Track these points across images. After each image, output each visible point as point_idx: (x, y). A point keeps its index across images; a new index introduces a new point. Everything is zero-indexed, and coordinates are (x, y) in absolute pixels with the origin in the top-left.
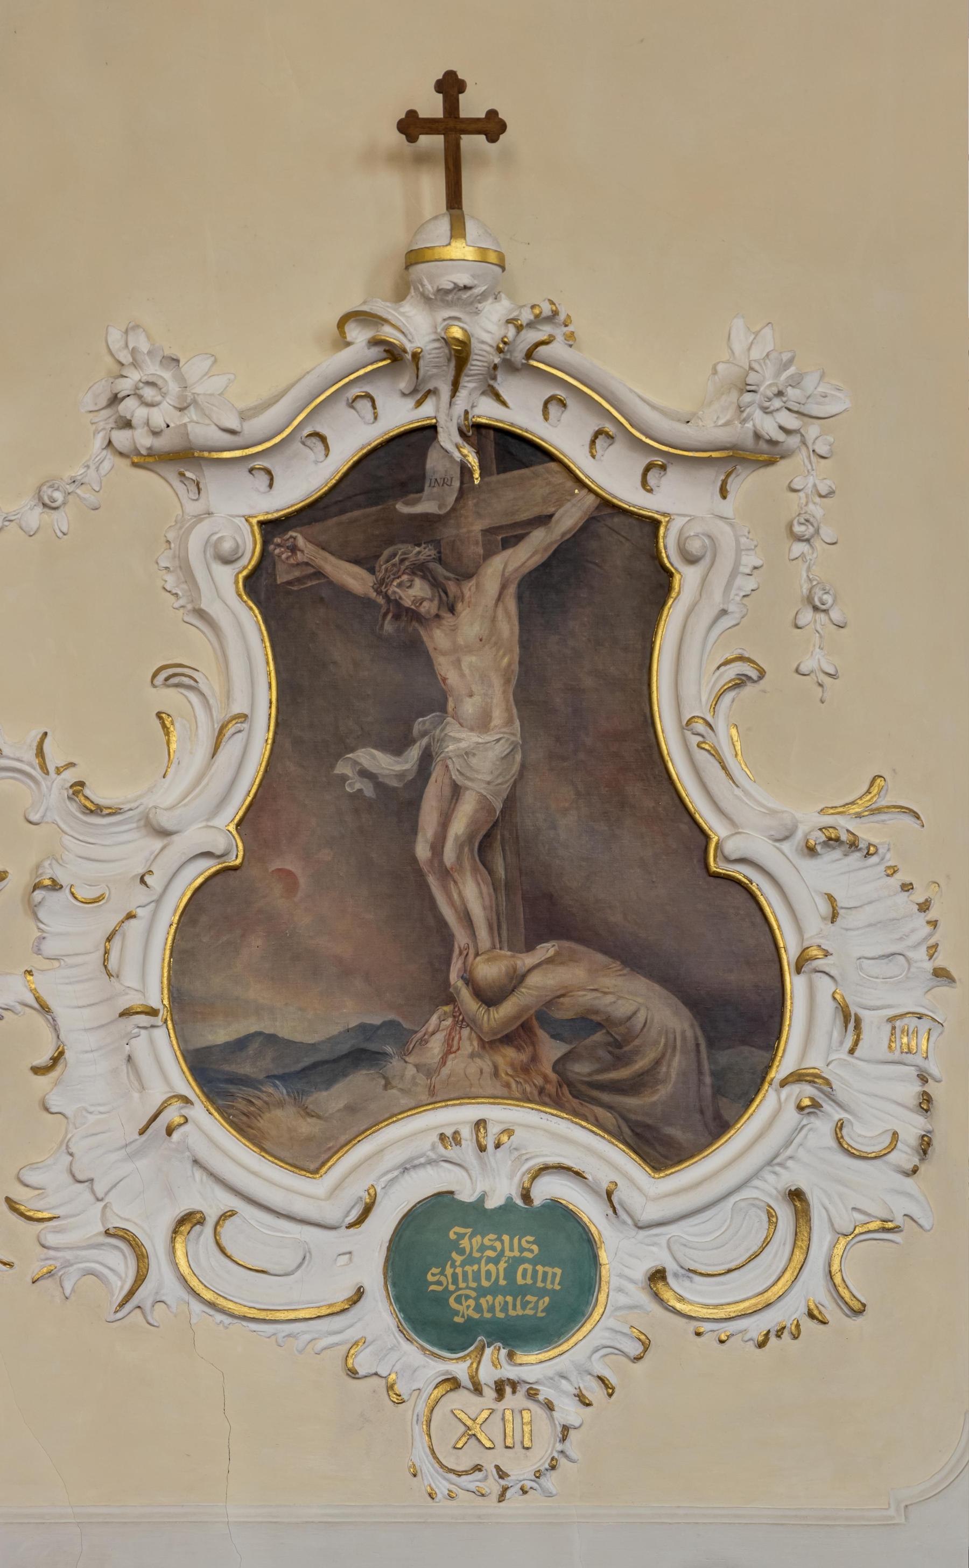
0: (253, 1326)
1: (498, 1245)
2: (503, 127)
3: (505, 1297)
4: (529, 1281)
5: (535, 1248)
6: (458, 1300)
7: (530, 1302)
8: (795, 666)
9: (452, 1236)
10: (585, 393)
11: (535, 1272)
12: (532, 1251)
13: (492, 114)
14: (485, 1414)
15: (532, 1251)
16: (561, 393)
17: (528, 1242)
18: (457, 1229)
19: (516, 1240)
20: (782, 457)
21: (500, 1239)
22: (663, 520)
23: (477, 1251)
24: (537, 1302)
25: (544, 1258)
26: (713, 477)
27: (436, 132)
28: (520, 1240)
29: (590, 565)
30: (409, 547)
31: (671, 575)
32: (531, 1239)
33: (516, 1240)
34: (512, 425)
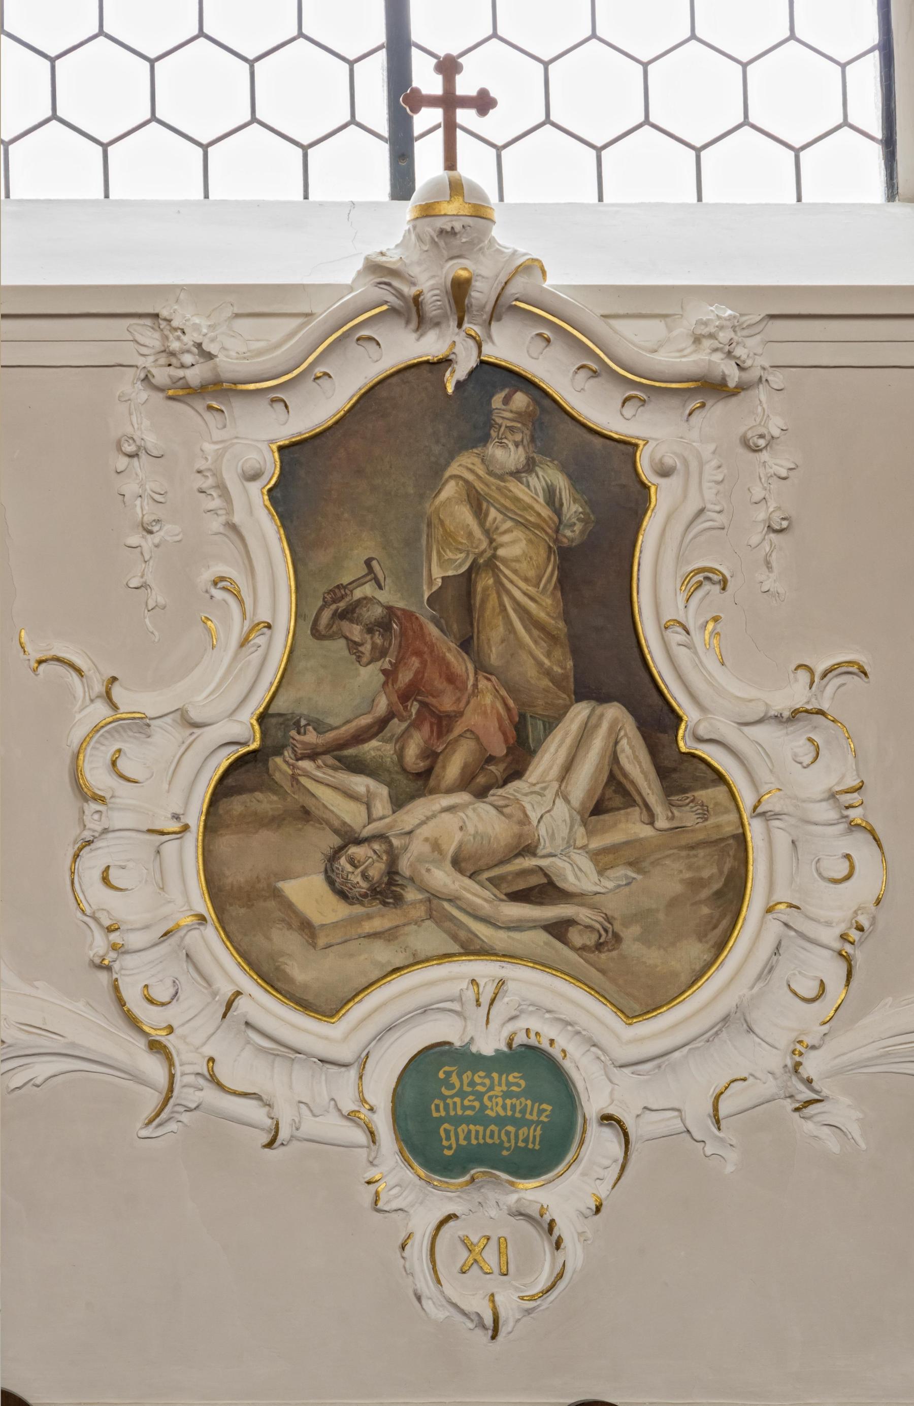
0: (572, 973)
1: (487, 1081)
5: (523, 1083)
7: (546, 1110)
8: (125, 583)
10: (569, 332)
12: (518, 1085)
15: (518, 1085)
16: (547, 333)
19: (504, 1076)
21: (488, 1076)
27: (454, 113)
28: (507, 1076)
31: (648, 488)
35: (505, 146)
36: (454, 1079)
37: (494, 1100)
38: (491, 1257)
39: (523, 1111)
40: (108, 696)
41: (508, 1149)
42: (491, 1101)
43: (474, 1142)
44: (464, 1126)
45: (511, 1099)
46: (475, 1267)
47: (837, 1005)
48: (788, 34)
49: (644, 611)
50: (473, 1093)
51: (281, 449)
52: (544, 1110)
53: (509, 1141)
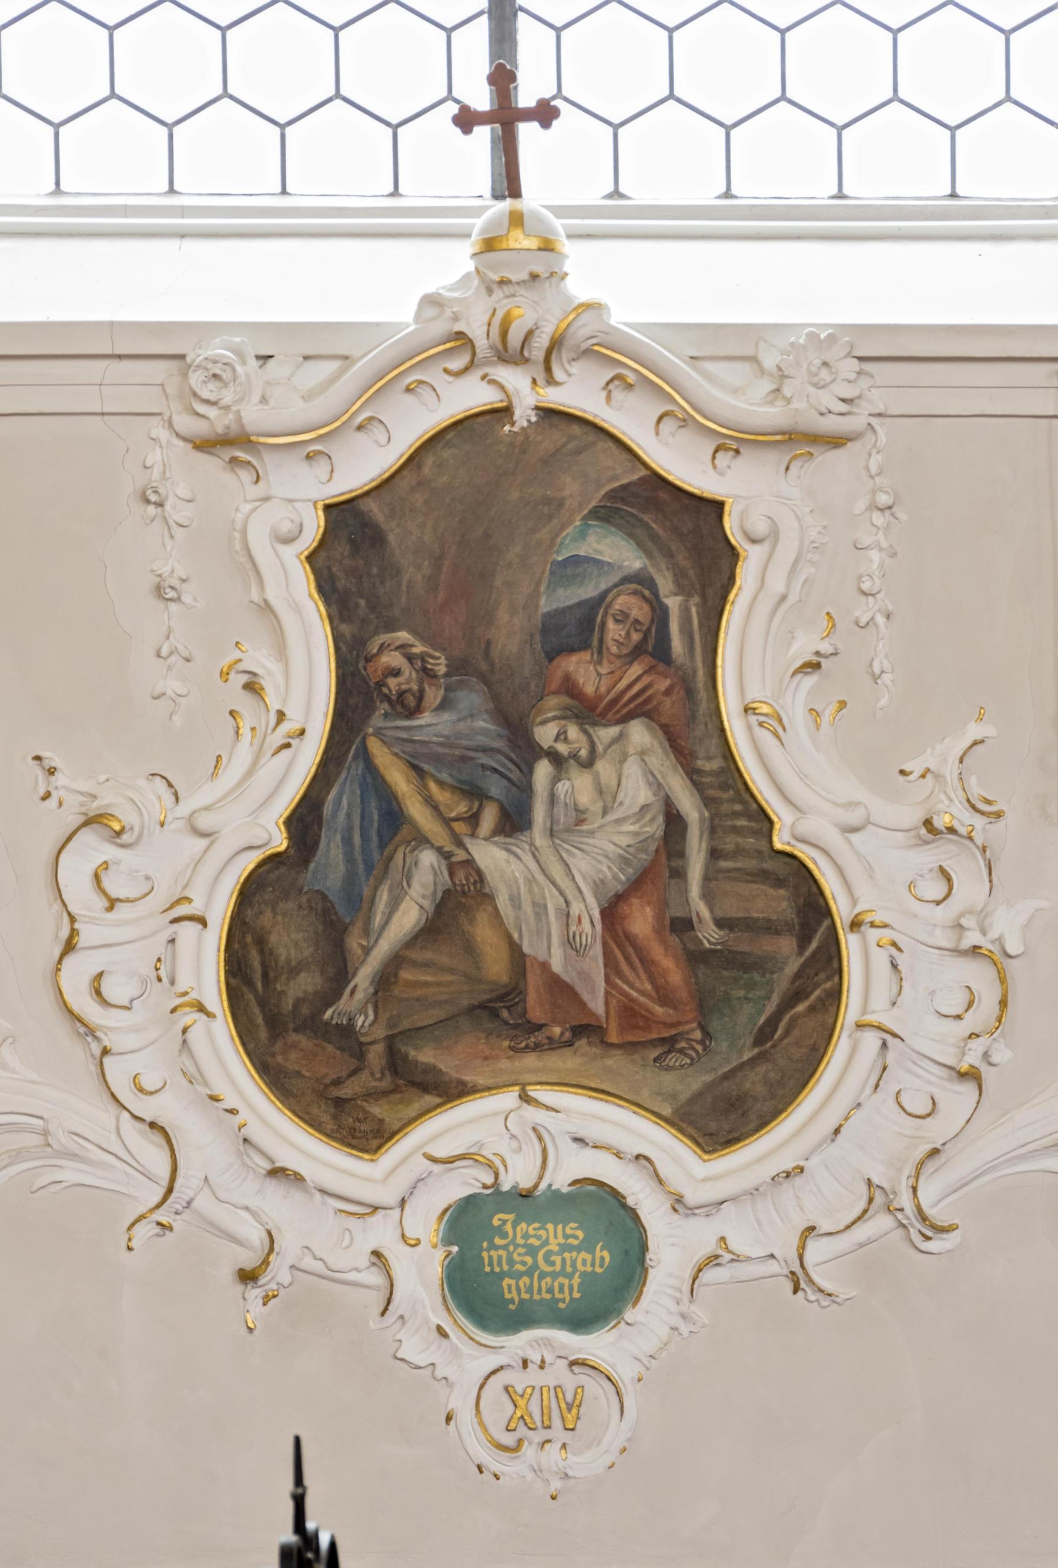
4: (506, 1268)
5: (581, 1234)
9: (496, 1222)
11: (564, 1260)
12: (576, 1237)
14: (529, 1390)
15: (576, 1237)
17: (572, 1229)
18: (499, 1216)
25: (588, 1246)
30: (443, 657)
32: (576, 1225)
33: (560, 1227)
35: (846, 126)
45: (570, 1252)
47: (756, 1282)
48: (106, 32)
50: (524, 1246)
51: (328, 508)
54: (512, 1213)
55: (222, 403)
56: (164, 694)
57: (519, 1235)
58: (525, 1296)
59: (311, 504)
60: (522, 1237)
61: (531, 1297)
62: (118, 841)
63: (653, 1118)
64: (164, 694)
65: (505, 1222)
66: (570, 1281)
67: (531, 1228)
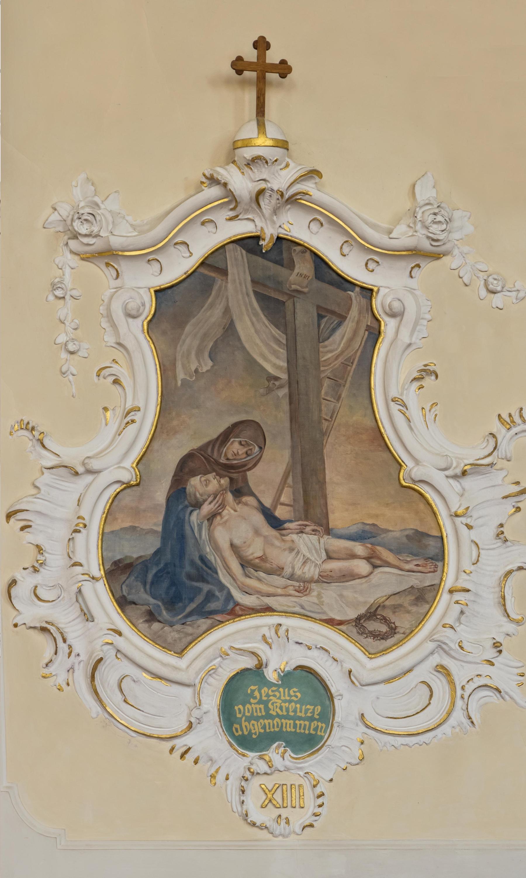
2: (262, 39)
3: (296, 705)
5: (299, 695)
6: (273, 704)
9: (249, 692)
12: (297, 697)
13: (283, 62)
15: (297, 697)
18: (253, 687)
20: (444, 255)
22: (375, 289)
23: (265, 696)
24: (314, 709)
26: (406, 265)
29: (127, 575)
32: (295, 690)
33: (286, 690)
34: (230, 238)
36: (257, 694)
37: (275, 705)
38: (278, 797)
39: (295, 711)
40: (464, 489)
41: (255, 734)
42: (273, 706)
43: (268, 730)
44: (315, 722)
46: (270, 804)
49: (380, 410)
51: (156, 291)
52: (309, 709)
53: (254, 729)
54: (256, 686)
55: (94, 234)
56: (428, 321)
57: (263, 695)
58: (312, 732)
59: (147, 290)
60: (265, 696)
61: (316, 733)
62: (263, 448)
63: (206, 634)
64: (428, 321)
65: (254, 691)
66: (273, 721)
67: (270, 691)
